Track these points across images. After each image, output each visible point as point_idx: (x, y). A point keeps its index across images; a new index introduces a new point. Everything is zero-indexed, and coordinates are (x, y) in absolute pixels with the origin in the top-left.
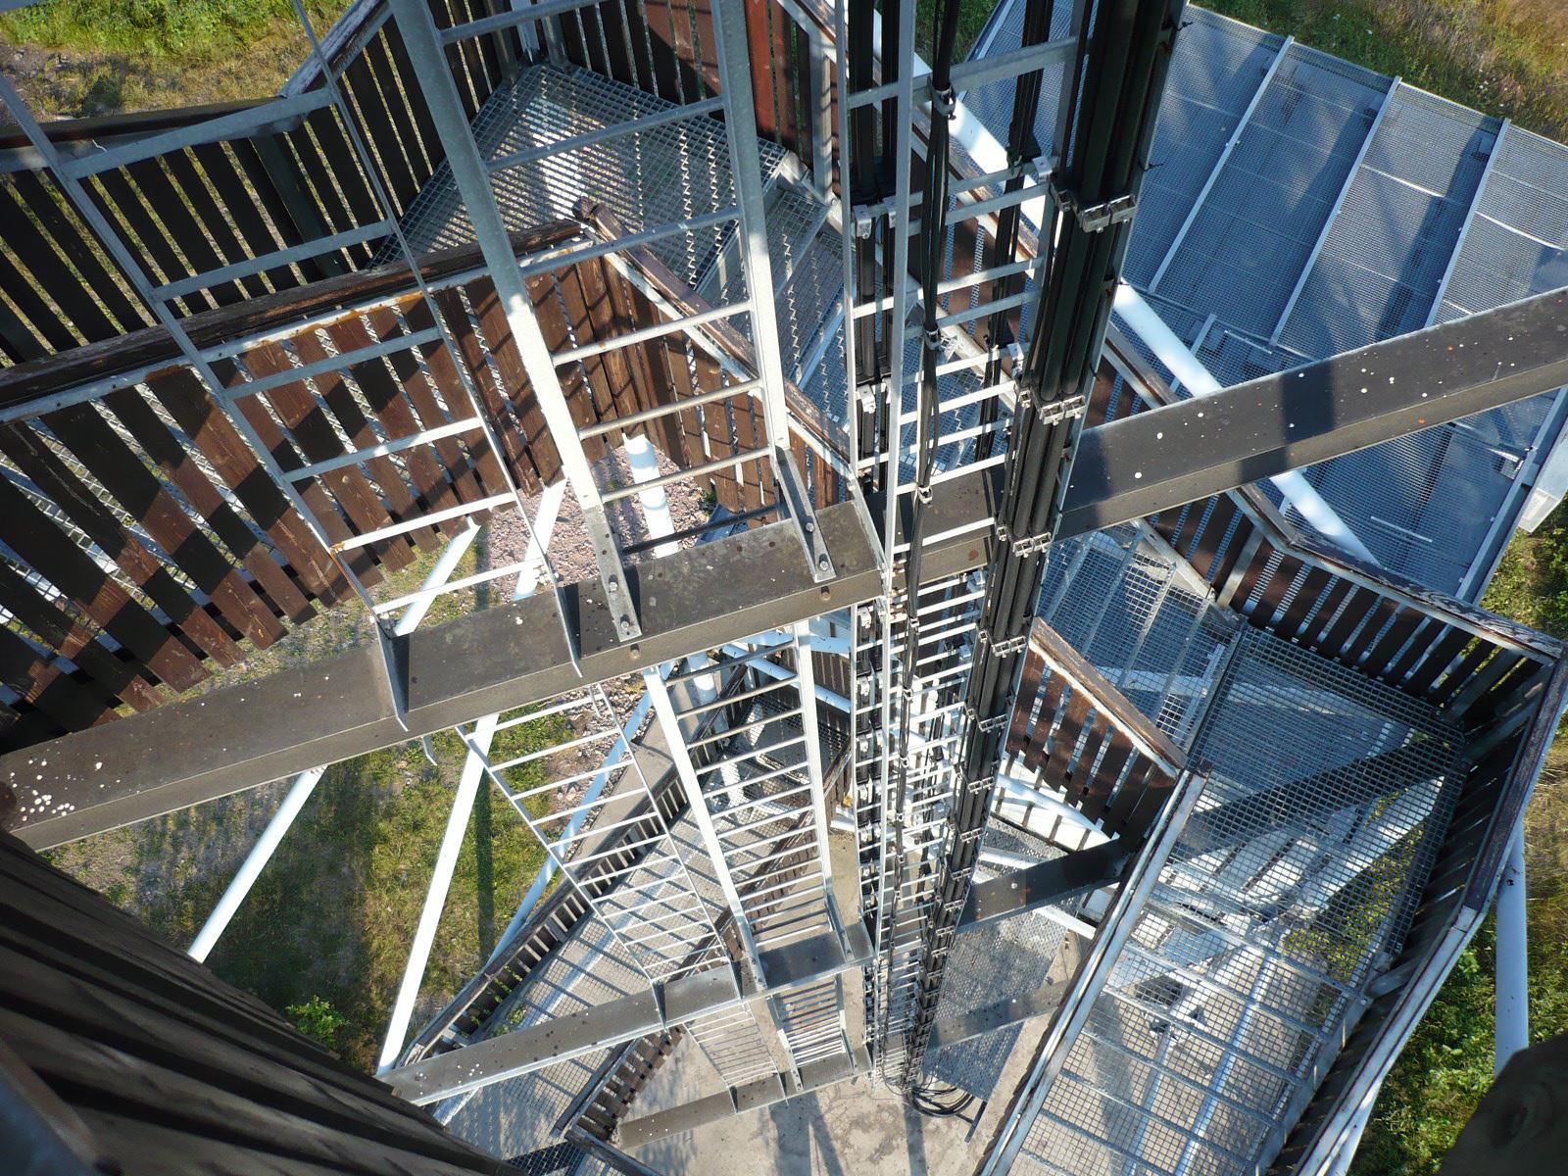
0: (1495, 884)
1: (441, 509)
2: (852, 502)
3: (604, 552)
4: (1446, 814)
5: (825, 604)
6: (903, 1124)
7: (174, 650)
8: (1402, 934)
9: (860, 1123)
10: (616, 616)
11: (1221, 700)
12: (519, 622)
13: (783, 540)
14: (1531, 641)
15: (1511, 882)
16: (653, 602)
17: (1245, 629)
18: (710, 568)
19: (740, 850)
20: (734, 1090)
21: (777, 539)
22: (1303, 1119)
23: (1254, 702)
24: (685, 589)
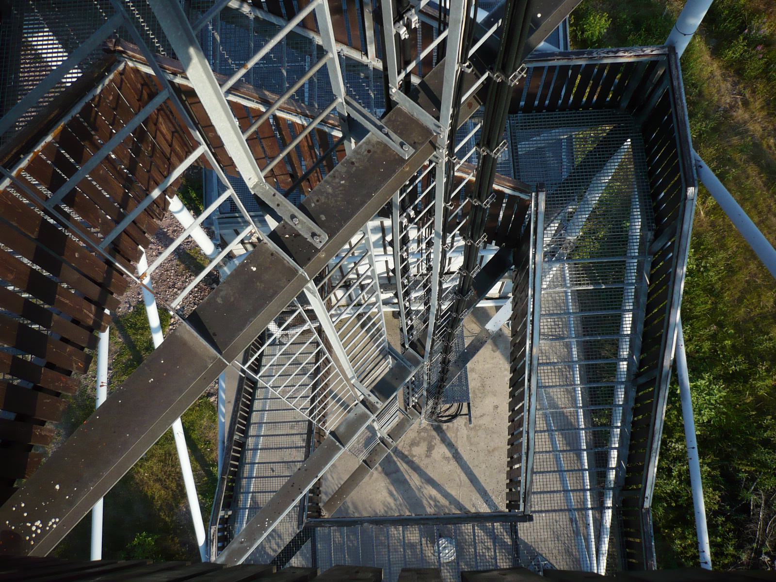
0: (695, 171)
1: (465, 94)
2: (398, 106)
3: (278, 205)
4: (643, 155)
5: (407, 172)
6: (434, 433)
7: (45, 400)
8: (652, 219)
9: (413, 444)
10: (307, 236)
11: (517, 156)
12: (254, 269)
13: (373, 146)
14: (652, 51)
15: (701, 167)
16: (323, 218)
17: (509, 117)
18: (343, 182)
19: (296, 355)
20: (364, 461)
21: (370, 148)
22: (645, 326)
23: (532, 149)
24: (336, 201)
